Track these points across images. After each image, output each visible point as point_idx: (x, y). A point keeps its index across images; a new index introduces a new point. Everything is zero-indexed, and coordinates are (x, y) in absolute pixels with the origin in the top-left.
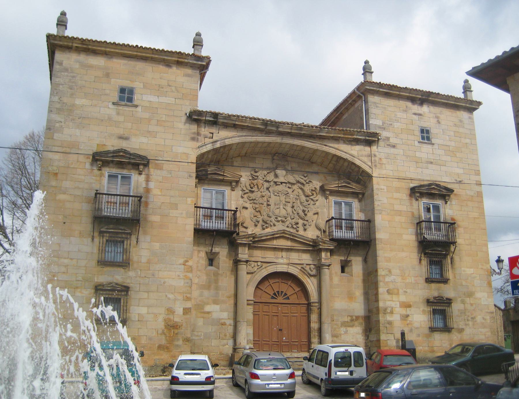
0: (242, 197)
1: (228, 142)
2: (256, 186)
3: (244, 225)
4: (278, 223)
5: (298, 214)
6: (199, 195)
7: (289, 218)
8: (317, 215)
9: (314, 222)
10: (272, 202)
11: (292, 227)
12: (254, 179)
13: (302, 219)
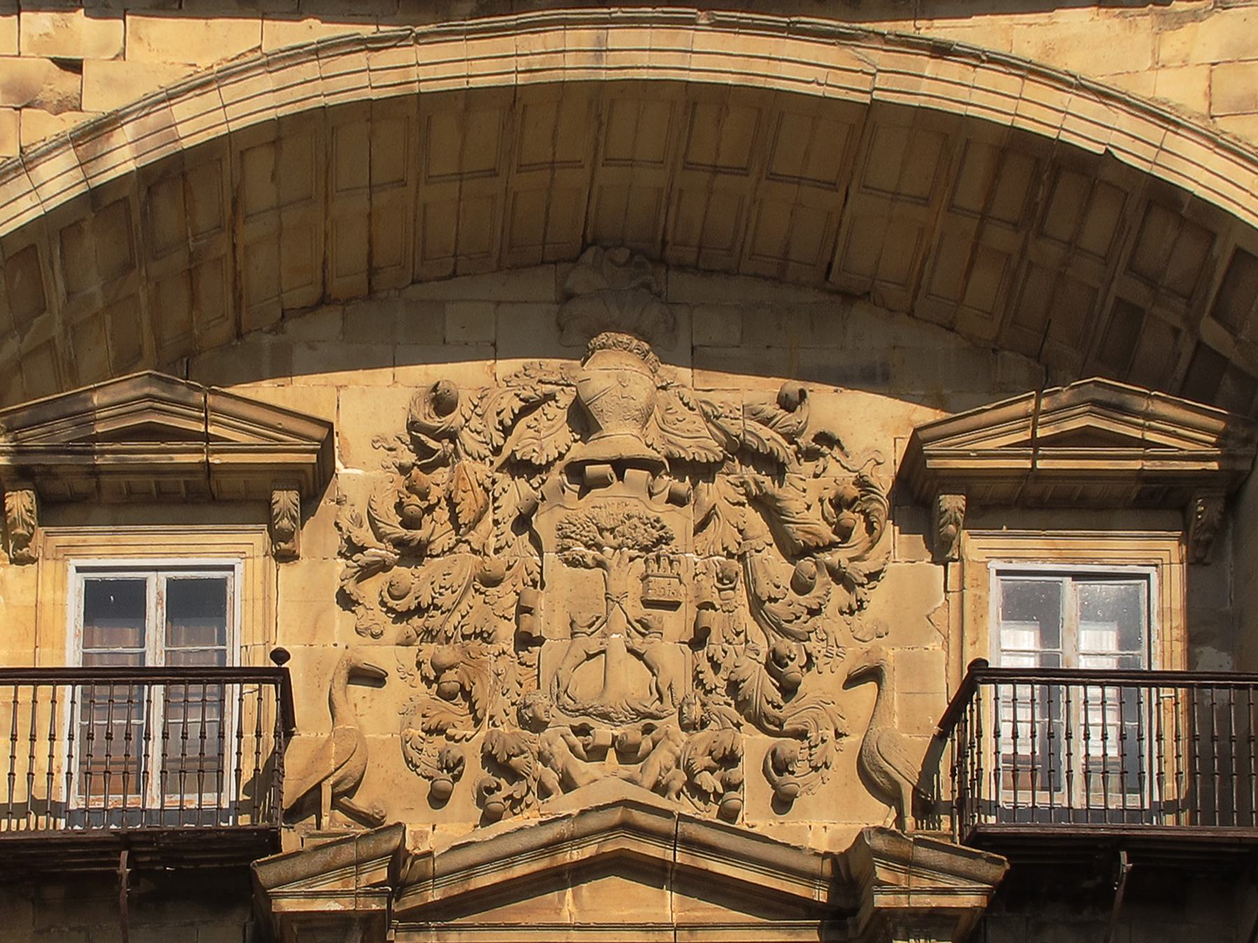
0: (346, 601)
1: (196, 122)
2: (443, 514)
3: (360, 801)
4: (593, 768)
5: (733, 687)
6: (47, 613)
7: (671, 724)
8: (871, 686)
9: (853, 740)
10: (549, 619)
11: (696, 791)
12: (429, 460)
13: (759, 721)
